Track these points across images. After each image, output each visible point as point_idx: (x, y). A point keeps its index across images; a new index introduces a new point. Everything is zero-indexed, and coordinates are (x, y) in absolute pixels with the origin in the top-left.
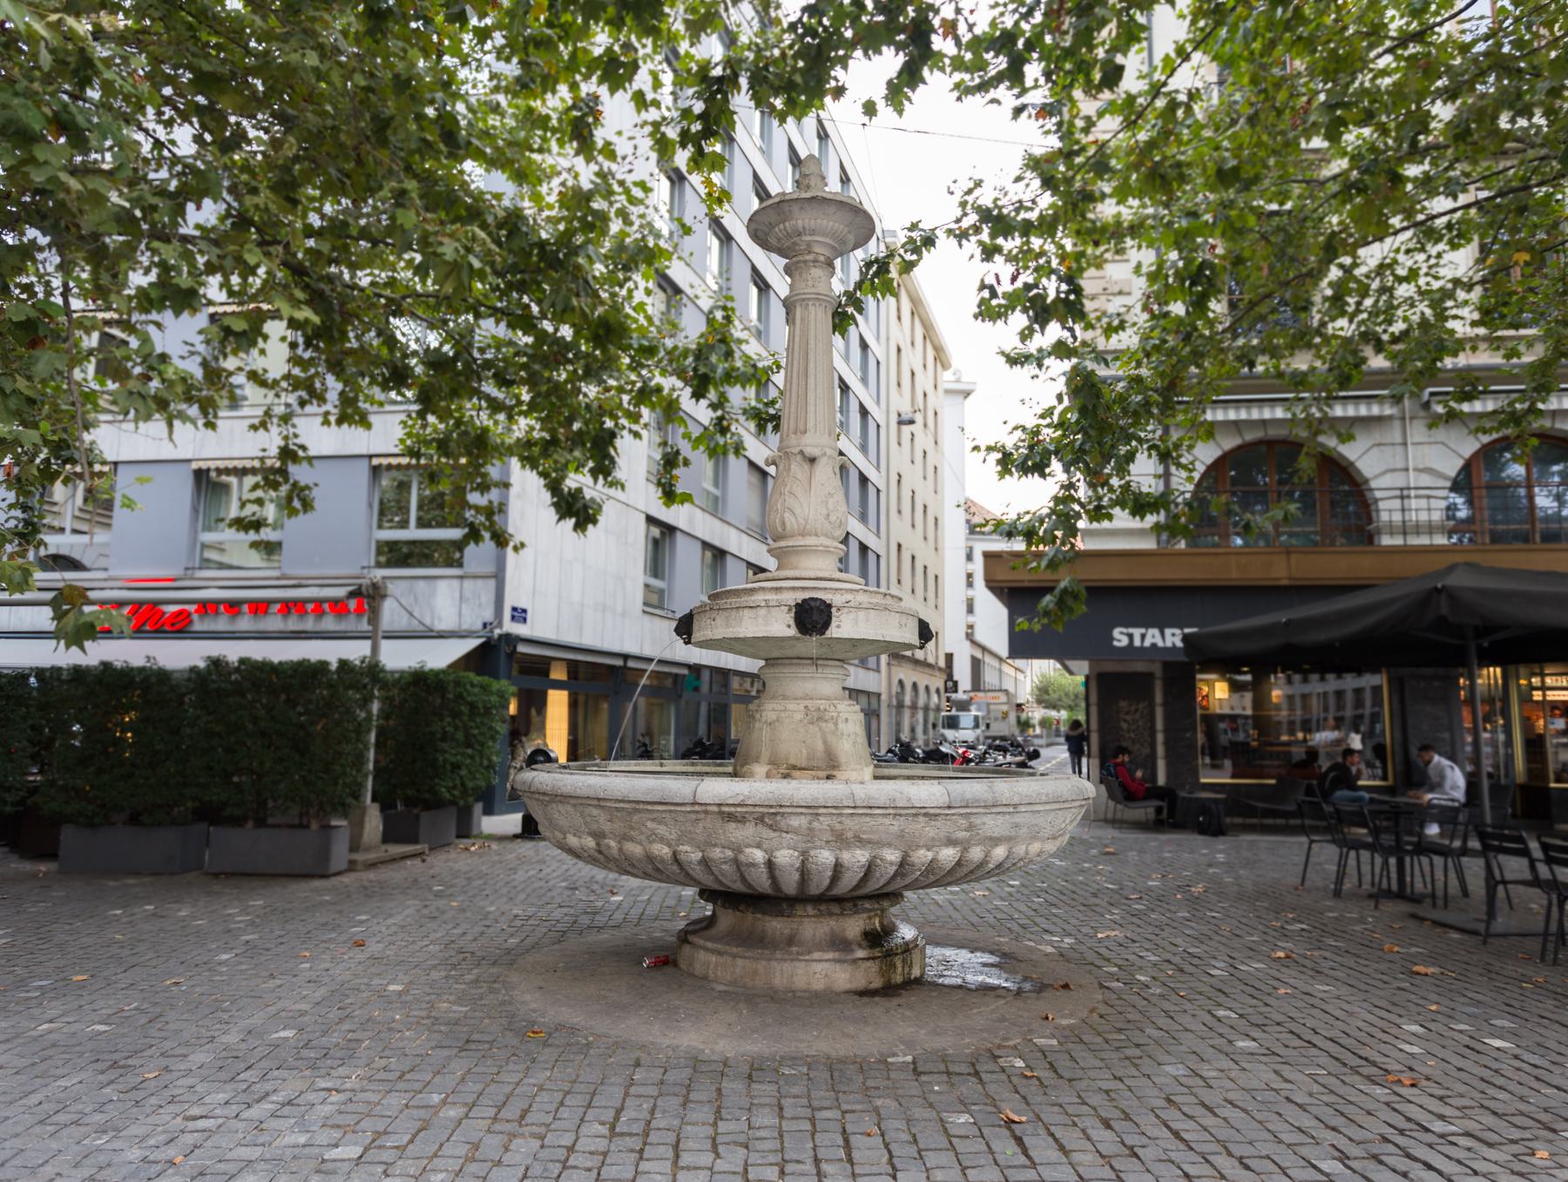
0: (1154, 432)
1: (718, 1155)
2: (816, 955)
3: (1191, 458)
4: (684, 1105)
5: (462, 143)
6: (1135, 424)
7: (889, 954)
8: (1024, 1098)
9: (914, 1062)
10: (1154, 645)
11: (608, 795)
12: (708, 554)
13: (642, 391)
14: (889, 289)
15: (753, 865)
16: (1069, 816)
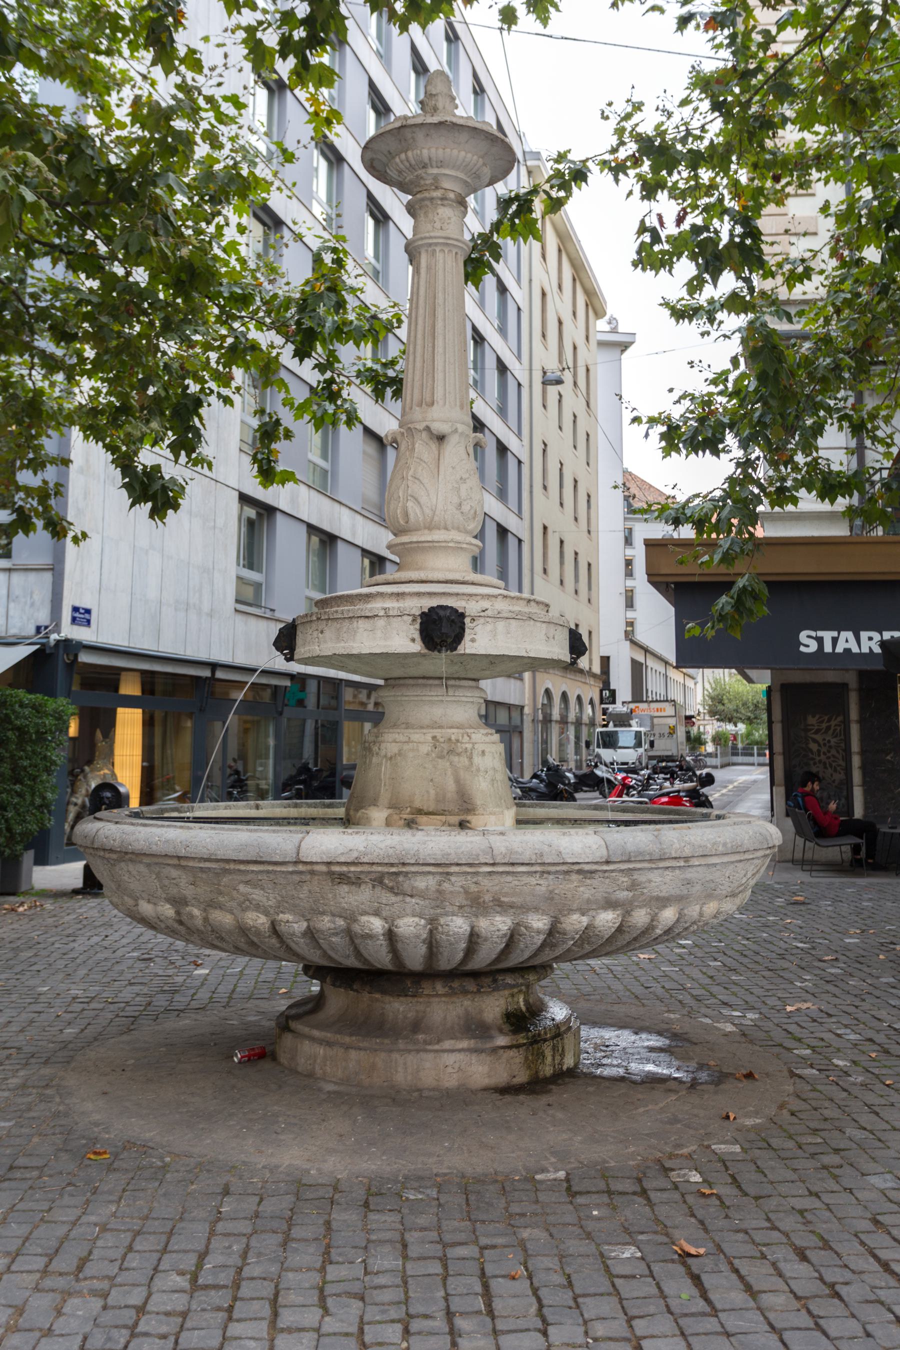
0: (845, 399)
1: (326, 1312)
2: (447, 1044)
3: (889, 430)
4: (284, 1244)
5: (11, 46)
6: (822, 392)
7: (536, 1040)
8: (702, 1222)
9: (568, 1179)
10: (847, 651)
11: (192, 851)
12: (315, 540)
13: (233, 348)
14: (530, 230)
15: (370, 936)
16: (751, 869)
